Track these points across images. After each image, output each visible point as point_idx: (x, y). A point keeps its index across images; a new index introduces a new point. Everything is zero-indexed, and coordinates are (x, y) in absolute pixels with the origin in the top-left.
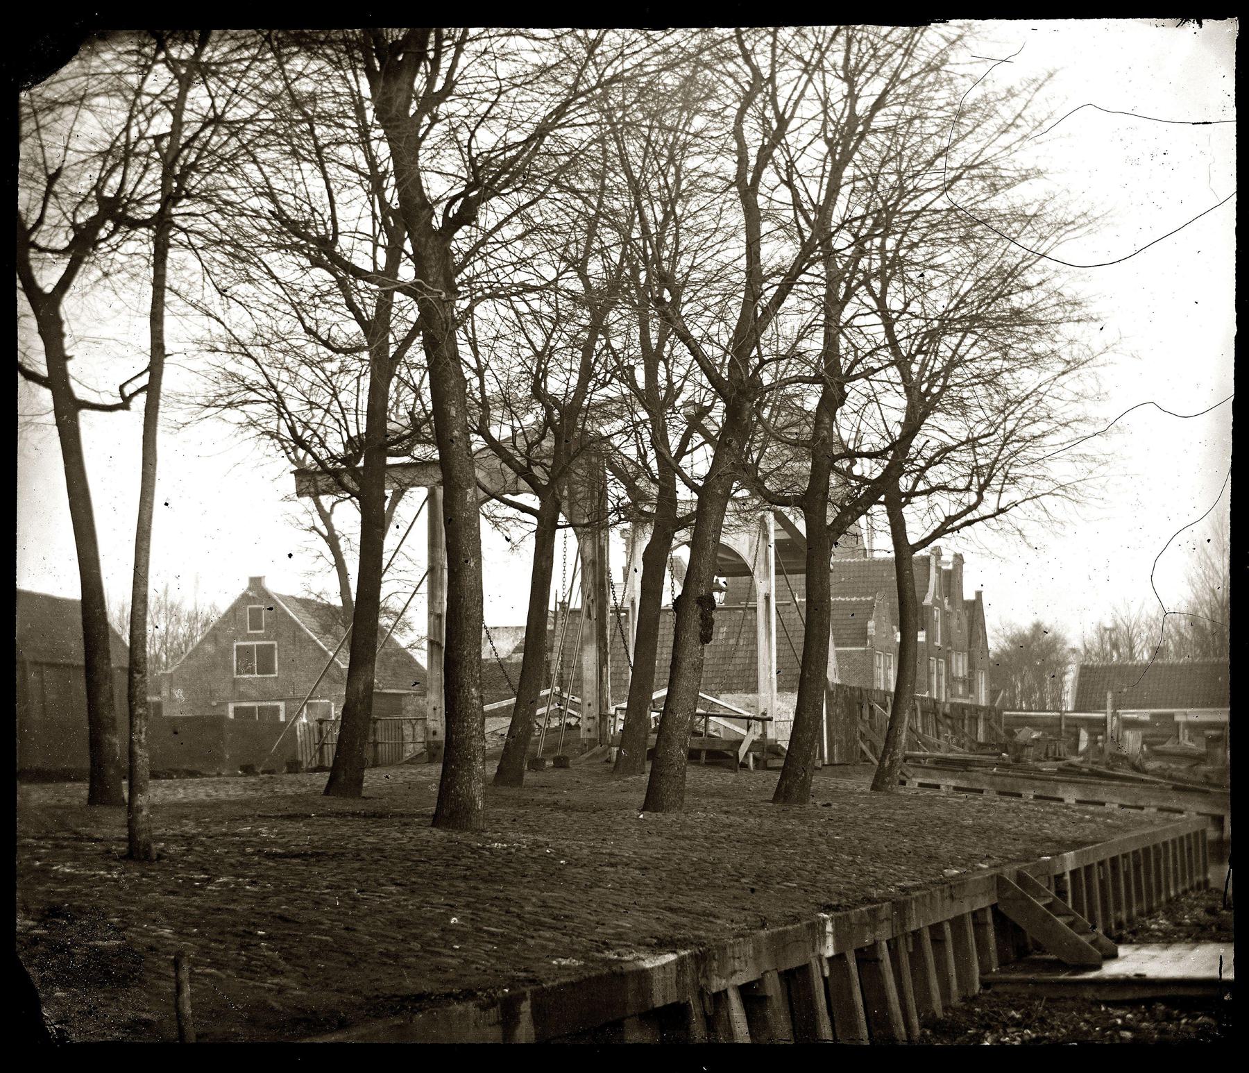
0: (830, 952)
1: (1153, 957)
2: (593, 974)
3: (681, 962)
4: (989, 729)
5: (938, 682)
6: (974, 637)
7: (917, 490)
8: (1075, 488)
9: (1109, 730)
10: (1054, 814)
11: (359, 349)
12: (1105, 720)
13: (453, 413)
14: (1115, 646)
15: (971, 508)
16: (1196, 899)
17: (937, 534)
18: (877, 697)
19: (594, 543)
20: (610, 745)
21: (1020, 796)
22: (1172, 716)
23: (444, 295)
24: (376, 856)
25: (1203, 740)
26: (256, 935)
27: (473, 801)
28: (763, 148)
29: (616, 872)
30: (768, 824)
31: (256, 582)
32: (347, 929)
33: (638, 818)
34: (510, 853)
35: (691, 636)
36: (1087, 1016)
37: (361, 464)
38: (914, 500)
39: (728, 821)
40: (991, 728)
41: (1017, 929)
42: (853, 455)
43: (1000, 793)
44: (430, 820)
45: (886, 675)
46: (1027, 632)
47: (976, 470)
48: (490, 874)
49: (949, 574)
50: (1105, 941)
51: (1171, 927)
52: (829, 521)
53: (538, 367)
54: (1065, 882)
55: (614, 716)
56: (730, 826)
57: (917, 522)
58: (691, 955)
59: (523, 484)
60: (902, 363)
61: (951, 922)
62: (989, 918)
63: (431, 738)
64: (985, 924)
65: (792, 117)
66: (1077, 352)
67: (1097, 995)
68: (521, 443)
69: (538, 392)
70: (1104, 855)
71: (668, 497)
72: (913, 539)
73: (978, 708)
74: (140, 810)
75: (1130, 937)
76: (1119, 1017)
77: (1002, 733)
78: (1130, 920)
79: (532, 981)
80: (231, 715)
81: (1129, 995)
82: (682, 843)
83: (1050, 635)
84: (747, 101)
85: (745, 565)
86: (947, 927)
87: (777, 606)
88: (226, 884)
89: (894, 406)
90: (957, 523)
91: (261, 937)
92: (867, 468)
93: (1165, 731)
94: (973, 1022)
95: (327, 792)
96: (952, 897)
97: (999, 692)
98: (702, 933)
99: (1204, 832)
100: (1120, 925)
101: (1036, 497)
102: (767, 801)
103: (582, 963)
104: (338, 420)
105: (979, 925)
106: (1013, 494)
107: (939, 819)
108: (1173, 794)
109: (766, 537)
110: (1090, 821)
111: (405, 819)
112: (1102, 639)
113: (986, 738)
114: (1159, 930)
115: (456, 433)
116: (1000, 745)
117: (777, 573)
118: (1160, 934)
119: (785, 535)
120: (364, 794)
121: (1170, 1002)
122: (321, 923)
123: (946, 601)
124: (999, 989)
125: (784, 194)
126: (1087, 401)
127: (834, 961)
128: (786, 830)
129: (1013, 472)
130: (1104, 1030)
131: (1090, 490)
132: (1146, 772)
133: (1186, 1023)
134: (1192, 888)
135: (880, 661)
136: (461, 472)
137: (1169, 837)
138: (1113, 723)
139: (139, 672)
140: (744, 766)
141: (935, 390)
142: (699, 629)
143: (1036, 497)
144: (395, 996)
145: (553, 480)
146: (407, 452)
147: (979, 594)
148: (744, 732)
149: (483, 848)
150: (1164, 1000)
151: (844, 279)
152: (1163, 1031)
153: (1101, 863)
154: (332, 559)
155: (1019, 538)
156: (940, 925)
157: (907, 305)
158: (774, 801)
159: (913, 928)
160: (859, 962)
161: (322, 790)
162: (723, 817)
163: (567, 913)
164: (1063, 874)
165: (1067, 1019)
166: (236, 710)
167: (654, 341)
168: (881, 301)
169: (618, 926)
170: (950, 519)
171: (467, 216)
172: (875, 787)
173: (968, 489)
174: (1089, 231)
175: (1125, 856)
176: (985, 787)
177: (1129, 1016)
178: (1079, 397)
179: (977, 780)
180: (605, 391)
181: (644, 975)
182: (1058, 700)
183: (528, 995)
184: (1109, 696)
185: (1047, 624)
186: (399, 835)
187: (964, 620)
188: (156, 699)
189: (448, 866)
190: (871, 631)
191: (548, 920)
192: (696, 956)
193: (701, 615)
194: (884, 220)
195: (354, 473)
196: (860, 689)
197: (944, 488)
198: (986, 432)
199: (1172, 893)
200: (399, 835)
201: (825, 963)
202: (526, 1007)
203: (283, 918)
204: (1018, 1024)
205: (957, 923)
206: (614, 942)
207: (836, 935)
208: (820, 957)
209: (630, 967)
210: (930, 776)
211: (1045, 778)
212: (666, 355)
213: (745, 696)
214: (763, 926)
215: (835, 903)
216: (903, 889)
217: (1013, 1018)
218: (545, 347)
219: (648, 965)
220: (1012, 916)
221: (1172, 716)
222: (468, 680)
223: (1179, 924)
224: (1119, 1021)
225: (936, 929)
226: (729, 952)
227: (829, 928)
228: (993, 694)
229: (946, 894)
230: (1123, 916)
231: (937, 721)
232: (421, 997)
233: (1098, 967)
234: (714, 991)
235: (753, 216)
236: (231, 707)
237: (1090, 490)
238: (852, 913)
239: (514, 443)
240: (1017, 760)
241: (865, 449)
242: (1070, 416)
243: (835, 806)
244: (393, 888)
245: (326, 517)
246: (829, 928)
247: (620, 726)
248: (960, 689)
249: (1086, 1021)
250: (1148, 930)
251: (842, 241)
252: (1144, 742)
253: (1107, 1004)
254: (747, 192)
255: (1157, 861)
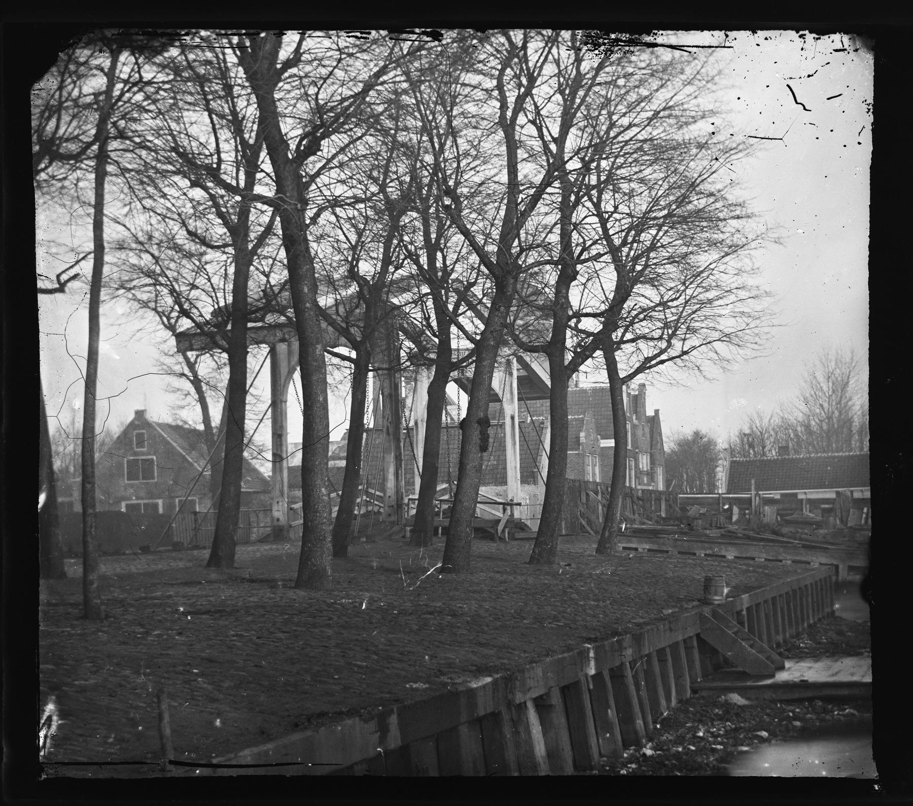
0: (592, 672)
1: (810, 668)
2: (438, 694)
3: (495, 683)
4: (669, 506)
5: (630, 475)
6: (654, 442)
7: (625, 339)
8: (736, 336)
9: (753, 507)
10: (728, 567)
11: (226, 245)
12: (750, 499)
13: (306, 290)
14: (751, 446)
15: (662, 352)
16: (828, 625)
17: (639, 371)
18: (591, 486)
19: (391, 381)
20: (405, 525)
21: (695, 554)
22: (796, 495)
23: (299, 206)
24: (262, 611)
25: (819, 511)
26: (193, 673)
27: (325, 570)
28: (519, 97)
29: (435, 619)
30: (531, 580)
31: (140, 414)
32: (256, 666)
33: (438, 578)
34: (355, 607)
35: (473, 449)
36: (768, 711)
37: (229, 327)
38: (623, 346)
39: (502, 579)
40: (670, 506)
41: (715, 651)
42: (579, 315)
43: (679, 553)
44: (293, 584)
45: (593, 470)
46: (690, 438)
47: (666, 325)
48: (347, 622)
49: (636, 397)
50: (776, 657)
51: (814, 645)
52: (566, 363)
53: (353, 256)
54: (743, 616)
55: (408, 505)
56: (505, 582)
57: (626, 360)
58: (502, 678)
59: (343, 340)
60: (614, 251)
61: (669, 646)
62: (695, 644)
63: (276, 523)
64: (693, 647)
65: (539, 75)
66: (738, 239)
67: (774, 696)
68: (341, 309)
69: (353, 274)
70: (769, 596)
71: (445, 346)
72: (622, 374)
73: (660, 493)
74: (92, 583)
75: (787, 653)
76: (790, 711)
77: (677, 509)
78: (785, 641)
79: (397, 701)
80: (123, 510)
81: (796, 695)
82: (475, 595)
83: (705, 439)
84: (506, 64)
85: (497, 395)
86: (668, 650)
87: (520, 422)
88: (159, 636)
89: (609, 278)
90: (653, 362)
91: (196, 674)
92: (592, 325)
93: (793, 506)
94: (689, 718)
95: (209, 564)
96: (671, 630)
97: (672, 481)
98: (506, 661)
99: (830, 577)
100: (778, 645)
101: (709, 343)
102: (526, 563)
103: (427, 686)
104: (212, 297)
105: (688, 649)
106: (693, 341)
107: (649, 573)
108: (802, 551)
109: (511, 374)
110: (753, 571)
111: (271, 584)
112: (742, 441)
113: (666, 514)
114: (806, 648)
115: (308, 305)
116: (677, 519)
117: (519, 399)
118: (806, 650)
119: (523, 373)
120: (235, 565)
121: (827, 699)
122: (237, 663)
123: (634, 417)
124: (704, 694)
125: (532, 130)
126: (745, 274)
127: (598, 677)
128: (545, 584)
129: (696, 325)
130: (781, 721)
131: (747, 337)
132: (783, 536)
133: (838, 714)
134: (824, 617)
135: (589, 460)
136: (312, 333)
137: (808, 582)
138: (756, 502)
139: (89, 483)
140: (502, 539)
141: (639, 268)
142: (479, 441)
143: (709, 343)
144: (302, 715)
145: (365, 337)
146: (262, 319)
147: (657, 412)
148: (501, 515)
149: (335, 603)
150: (820, 698)
151: (573, 192)
152: (822, 720)
153: (766, 602)
154: (197, 396)
155: (697, 371)
156: (663, 649)
157: (616, 207)
158: (530, 563)
159: (647, 652)
160: (611, 677)
161: (205, 562)
162: (498, 576)
163: (408, 649)
164: (742, 610)
165: (754, 713)
166: (127, 506)
167: (433, 236)
168: (597, 205)
169: (446, 658)
170: (648, 359)
171: (313, 148)
172: (598, 550)
173: (661, 338)
174: (747, 155)
175: (780, 596)
176: (670, 549)
177: (798, 710)
178: (739, 272)
179: (664, 544)
180: (400, 271)
181: (471, 693)
182: (712, 487)
183: (395, 710)
184: (753, 482)
185: (704, 431)
186: (272, 596)
187: (647, 430)
188: (66, 499)
189: (314, 617)
190: (583, 439)
191: (397, 655)
192: (505, 678)
193: (481, 432)
194: (599, 148)
195: (225, 335)
196: (579, 481)
197: (644, 337)
198: (674, 296)
199: (811, 622)
200: (272, 596)
201: (590, 680)
202: (393, 720)
203: (210, 660)
204: (721, 718)
205: (674, 647)
206: (446, 670)
207: (597, 659)
208: (586, 675)
209: (461, 688)
210: (630, 542)
211: (711, 541)
212: (442, 246)
213: (494, 487)
214: (547, 655)
215: (593, 636)
216: (638, 625)
217: (717, 714)
218: (357, 242)
219: (474, 685)
220: (711, 640)
221: (796, 495)
222: (319, 482)
223: (819, 643)
224: (791, 714)
225: (661, 652)
226: (527, 675)
227: (592, 654)
228: (668, 483)
229: (667, 627)
230: (780, 638)
231: (633, 502)
232: (322, 715)
233: (773, 676)
234: (518, 702)
235: (512, 145)
236: (123, 504)
237: (747, 337)
238: (606, 643)
239: (337, 310)
240: (691, 529)
241: (589, 310)
242: (734, 286)
243: (574, 565)
244: (281, 635)
245: (191, 366)
246: (592, 654)
247: (413, 512)
248: (645, 479)
249: (768, 715)
250: (799, 647)
251: (574, 165)
252: (778, 514)
253: (781, 701)
254: (508, 126)
255: (801, 599)
